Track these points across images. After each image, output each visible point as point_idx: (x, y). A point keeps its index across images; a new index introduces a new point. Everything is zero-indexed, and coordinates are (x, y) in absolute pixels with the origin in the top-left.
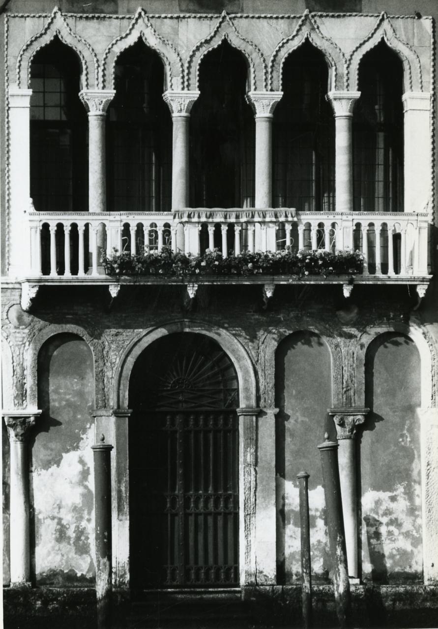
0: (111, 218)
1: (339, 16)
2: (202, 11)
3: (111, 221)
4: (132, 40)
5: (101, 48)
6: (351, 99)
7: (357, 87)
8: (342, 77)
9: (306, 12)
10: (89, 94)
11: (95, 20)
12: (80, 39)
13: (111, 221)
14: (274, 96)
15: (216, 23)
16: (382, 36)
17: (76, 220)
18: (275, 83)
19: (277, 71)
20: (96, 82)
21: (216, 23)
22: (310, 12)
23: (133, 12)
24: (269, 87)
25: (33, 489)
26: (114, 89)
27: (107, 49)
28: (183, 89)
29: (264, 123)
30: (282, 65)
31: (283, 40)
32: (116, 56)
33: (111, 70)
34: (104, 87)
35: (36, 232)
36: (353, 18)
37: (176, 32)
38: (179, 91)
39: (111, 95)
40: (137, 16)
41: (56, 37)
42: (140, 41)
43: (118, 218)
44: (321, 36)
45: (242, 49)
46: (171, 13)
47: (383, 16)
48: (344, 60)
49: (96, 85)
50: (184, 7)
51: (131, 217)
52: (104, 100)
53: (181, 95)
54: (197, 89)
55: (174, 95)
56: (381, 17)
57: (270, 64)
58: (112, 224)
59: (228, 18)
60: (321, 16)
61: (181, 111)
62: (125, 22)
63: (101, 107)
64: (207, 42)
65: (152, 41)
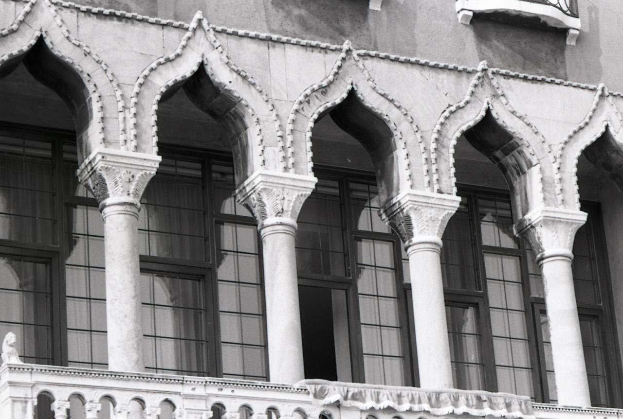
0: (186, 390)
1: (534, 80)
2: (308, 36)
3: (187, 397)
4: (186, 69)
5: (130, 73)
6: (572, 223)
7: (578, 205)
8: (552, 185)
9: (482, 65)
10: (109, 158)
11: (115, 22)
12: (88, 50)
13: (187, 397)
14: (446, 203)
15: (334, 60)
16: (605, 123)
17: (111, 388)
18: (444, 178)
19: (446, 160)
20: (122, 138)
21: (334, 60)
22: (490, 65)
23: (189, 19)
24: (436, 187)
25: (555, 387)
26: (159, 154)
27: (141, 76)
28: (286, 169)
29: (430, 254)
30: (452, 151)
31: (450, 106)
32: (159, 92)
33: (150, 119)
34: (137, 148)
35: (24, 410)
36: (547, 85)
37: (266, 67)
38: (279, 172)
39: (152, 164)
40: (193, 24)
41: (41, 40)
42: (201, 72)
43: (200, 391)
44: (396, 103)
45: (385, 113)
46: (428, 58)
47: (603, 89)
48: (551, 156)
49: (122, 142)
50: (275, 26)
51: (227, 391)
52: (138, 175)
53: (281, 181)
54: (312, 174)
55: (270, 180)
56: (599, 92)
57: (433, 146)
58: (188, 404)
59: (355, 53)
60: (506, 76)
61: (280, 213)
62: (173, 34)
63: (132, 187)
64: (324, 90)
65: (222, 75)
